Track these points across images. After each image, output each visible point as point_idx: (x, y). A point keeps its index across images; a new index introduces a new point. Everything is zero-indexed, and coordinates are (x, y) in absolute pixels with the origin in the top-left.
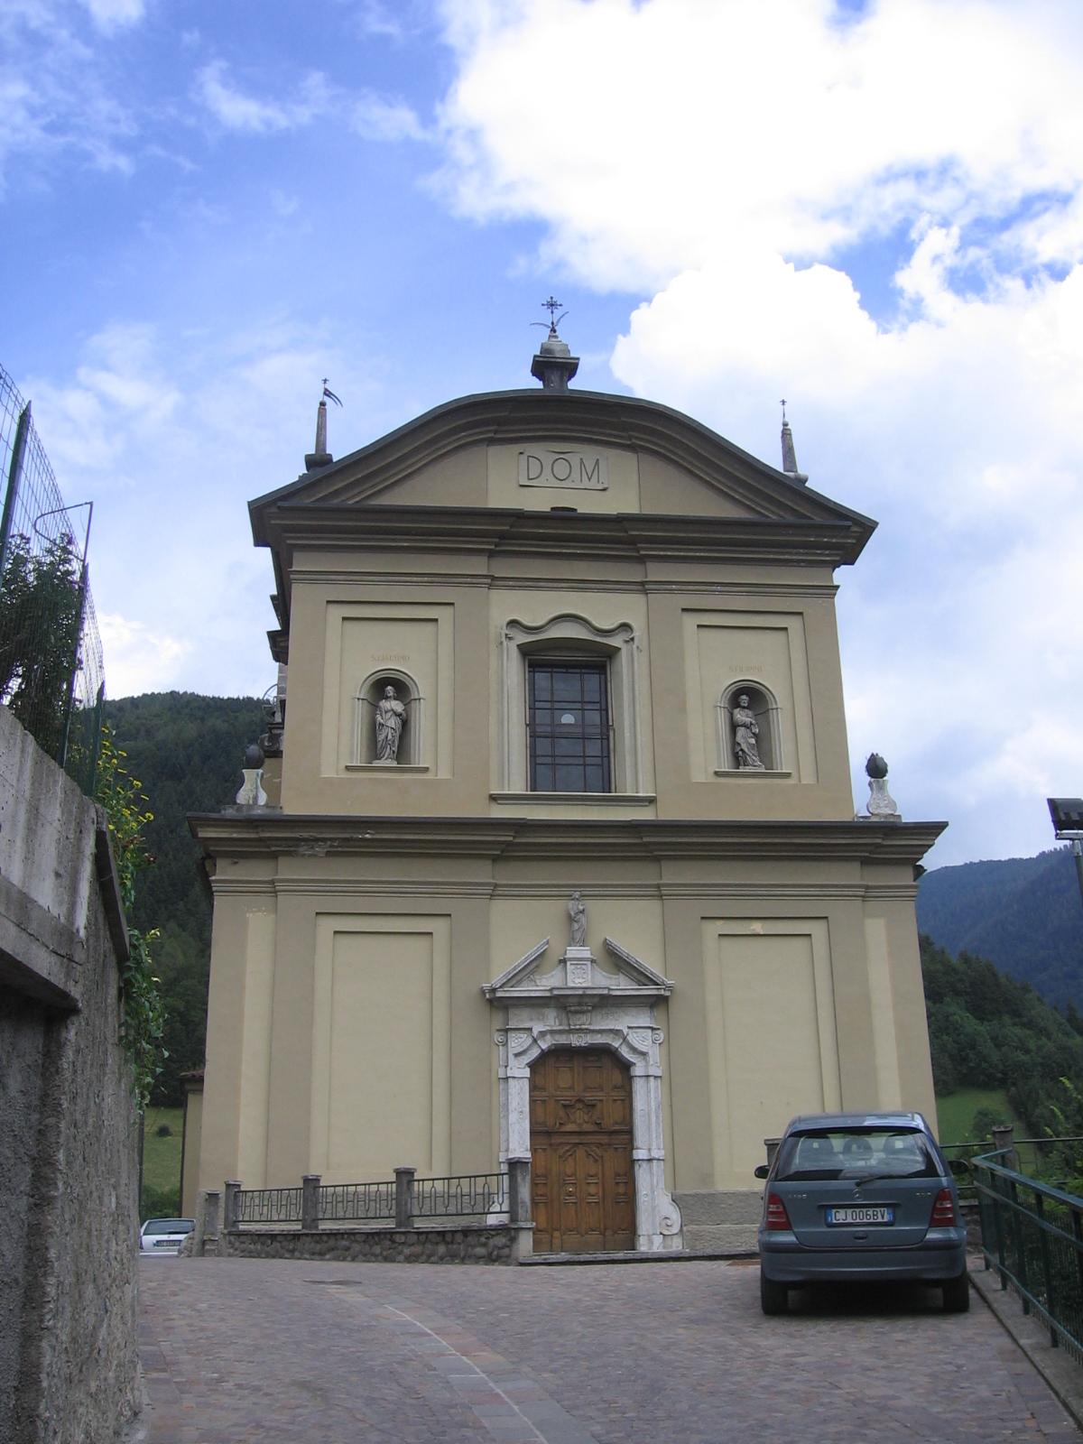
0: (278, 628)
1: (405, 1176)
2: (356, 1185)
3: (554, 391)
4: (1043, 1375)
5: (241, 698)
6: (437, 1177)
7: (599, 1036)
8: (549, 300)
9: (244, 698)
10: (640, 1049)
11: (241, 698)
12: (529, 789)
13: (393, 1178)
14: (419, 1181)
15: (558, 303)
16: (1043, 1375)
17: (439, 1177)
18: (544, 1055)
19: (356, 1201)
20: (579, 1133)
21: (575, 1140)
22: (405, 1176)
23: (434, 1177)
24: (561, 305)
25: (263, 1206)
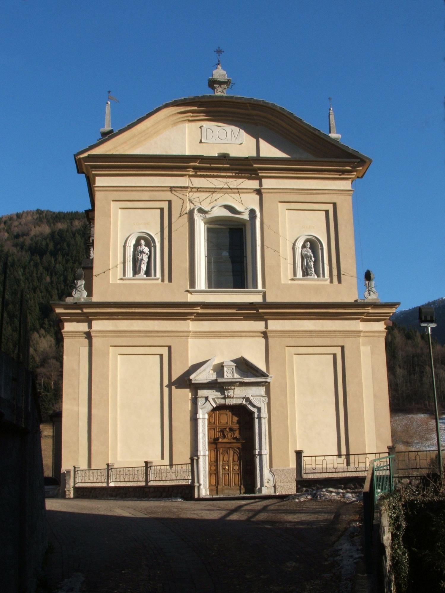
0: (91, 208)
1: (147, 464)
2: (160, 466)
3: (196, 174)
4: (157, 481)
5: (74, 212)
6: (360, 453)
7: (239, 400)
8: (218, 49)
9: (75, 212)
10: (257, 406)
11: (74, 212)
12: (207, 288)
13: (387, 450)
14: (175, 465)
15: (222, 51)
16: (157, 481)
17: (179, 464)
18: (214, 410)
19: (138, 474)
20: (230, 443)
21: (228, 445)
22: (147, 464)
23: (380, 452)
24: (223, 52)
25: (94, 476)
